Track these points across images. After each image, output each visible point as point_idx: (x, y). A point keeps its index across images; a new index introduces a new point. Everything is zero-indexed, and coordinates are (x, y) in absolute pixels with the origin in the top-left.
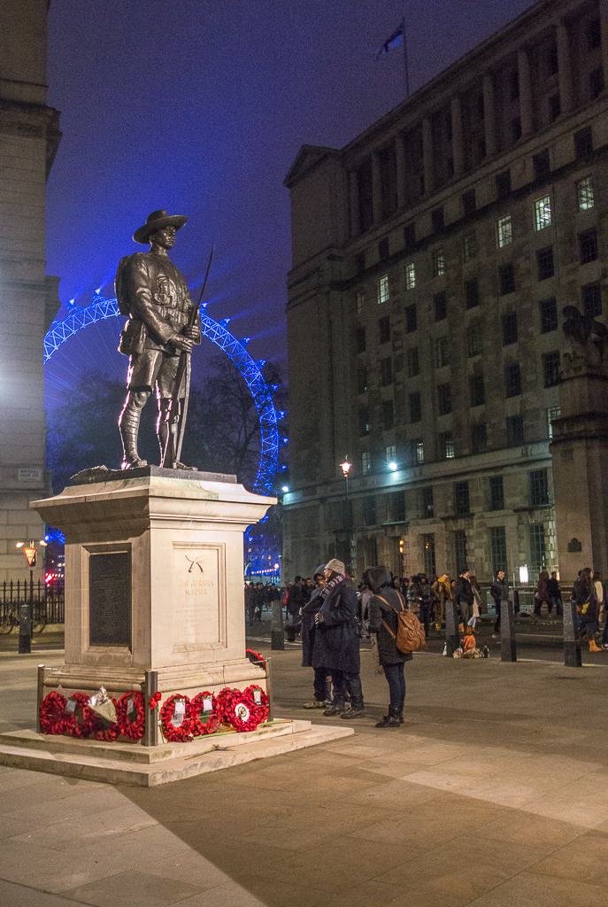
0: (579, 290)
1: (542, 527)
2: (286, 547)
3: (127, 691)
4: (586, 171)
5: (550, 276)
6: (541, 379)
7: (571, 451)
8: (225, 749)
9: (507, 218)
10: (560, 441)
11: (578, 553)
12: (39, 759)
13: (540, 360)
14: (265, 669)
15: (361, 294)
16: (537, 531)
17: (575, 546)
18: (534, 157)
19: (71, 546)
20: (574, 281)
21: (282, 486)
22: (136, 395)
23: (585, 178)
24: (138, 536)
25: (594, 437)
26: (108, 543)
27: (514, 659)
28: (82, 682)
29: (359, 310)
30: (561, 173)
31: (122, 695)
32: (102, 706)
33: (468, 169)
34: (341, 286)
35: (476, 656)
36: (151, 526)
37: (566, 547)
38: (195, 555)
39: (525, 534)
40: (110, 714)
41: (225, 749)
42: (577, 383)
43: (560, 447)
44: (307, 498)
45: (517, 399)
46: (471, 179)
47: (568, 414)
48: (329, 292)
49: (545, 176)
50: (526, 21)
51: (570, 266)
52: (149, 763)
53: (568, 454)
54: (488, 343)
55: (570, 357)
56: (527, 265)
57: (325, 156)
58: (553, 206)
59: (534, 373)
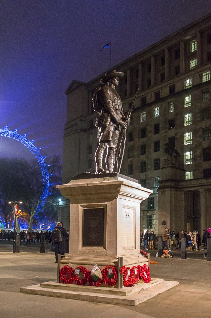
0: (167, 139)
1: (151, 217)
2: (59, 220)
3: (107, 266)
4: (173, 99)
5: (158, 133)
6: (153, 168)
7: (165, 192)
8: (146, 290)
9: (144, 113)
10: (161, 188)
11: (165, 225)
12: (71, 294)
13: (153, 160)
14: (147, 258)
15: (91, 134)
16: (149, 218)
17: (164, 223)
18: (155, 93)
19: (74, 205)
20: (166, 135)
21: (8, 203)
22: (103, 144)
23: (171, 102)
24: (111, 201)
25: (173, 187)
26: (94, 204)
27: (186, 259)
28: (79, 261)
29: (90, 140)
30: (164, 99)
31: (104, 267)
32: (96, 271)
33: (131, 94)
34: (85, 130)
35: (170, 257)
36: (118, 197)
37: (161, 223)
38: (127, 210)
39: (145, 219)
40: (100, 275)
41: (146, 290)
42: (168, 169)
43: (161, 190)
44: (67, 204)
45: (144, 174)
46: (132, 98)
47: (164, 179)
48: (80, 132)
49: (158, 100)
50: (154, 47)
51: (165, 130)
52: (126, 296)
53: (164, 192)
54: (135, 154)
55: (166, 160)
56: (151, 129)
57: (81, 85)
58: (160, 110)
59: (150, 165)
